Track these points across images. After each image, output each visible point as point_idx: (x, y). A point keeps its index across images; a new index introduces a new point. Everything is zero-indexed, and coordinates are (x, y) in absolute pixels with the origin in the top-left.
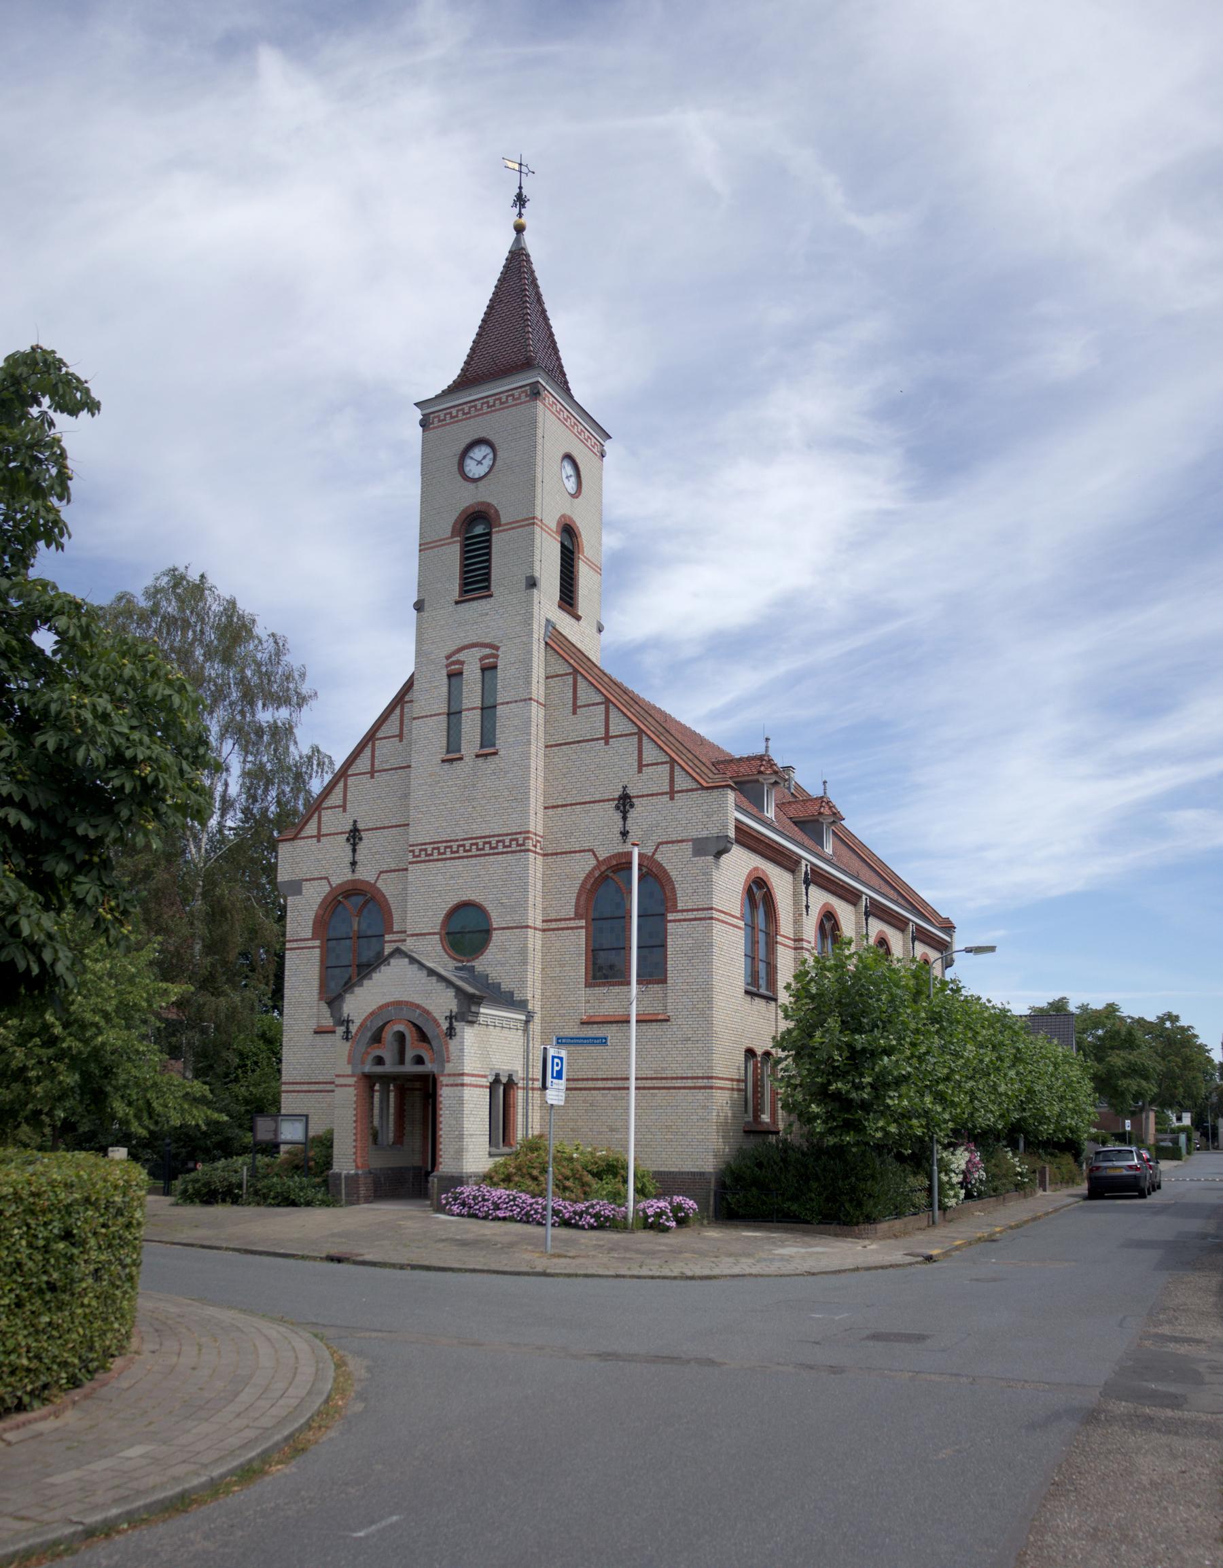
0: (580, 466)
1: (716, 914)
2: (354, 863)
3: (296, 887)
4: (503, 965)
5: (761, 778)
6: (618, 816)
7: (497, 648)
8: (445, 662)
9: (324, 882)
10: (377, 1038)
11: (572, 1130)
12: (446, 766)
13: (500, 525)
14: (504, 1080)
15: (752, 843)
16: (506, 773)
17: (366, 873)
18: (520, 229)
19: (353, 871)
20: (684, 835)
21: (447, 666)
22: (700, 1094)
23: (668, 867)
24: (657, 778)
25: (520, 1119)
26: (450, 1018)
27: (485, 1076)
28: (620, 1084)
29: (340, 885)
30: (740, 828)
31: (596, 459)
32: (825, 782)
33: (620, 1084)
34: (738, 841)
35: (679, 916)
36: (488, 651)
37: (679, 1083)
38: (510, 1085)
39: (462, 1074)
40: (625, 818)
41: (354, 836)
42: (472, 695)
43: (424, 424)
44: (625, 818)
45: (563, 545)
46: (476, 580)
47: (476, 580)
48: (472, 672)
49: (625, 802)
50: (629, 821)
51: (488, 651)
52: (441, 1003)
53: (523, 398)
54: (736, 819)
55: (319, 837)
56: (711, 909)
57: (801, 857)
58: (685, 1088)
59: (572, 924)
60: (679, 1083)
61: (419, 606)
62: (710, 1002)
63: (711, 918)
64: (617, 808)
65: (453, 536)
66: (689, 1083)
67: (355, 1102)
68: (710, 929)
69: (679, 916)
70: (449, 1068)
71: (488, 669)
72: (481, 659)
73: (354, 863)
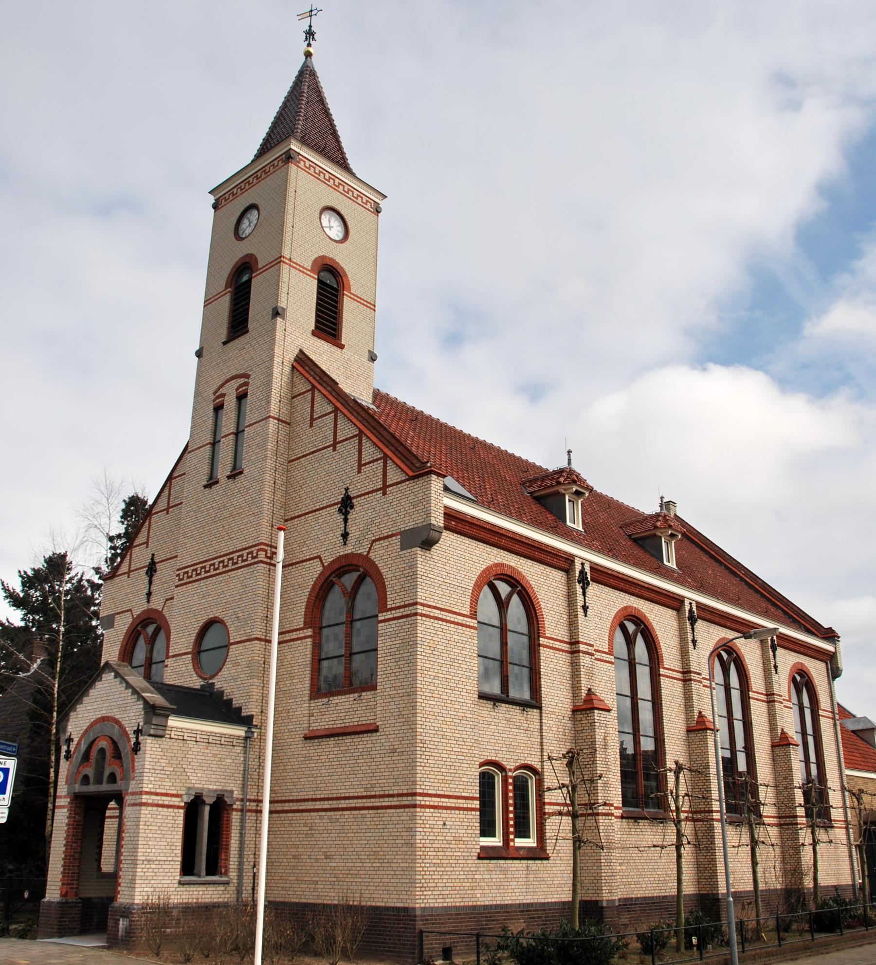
0: (342, 213)
1: (420, 609)
2: (149, 594)
3: (109, 622)
4: (235, 680)
5: (561, 489)
6: (340, 518)
7: (247, 376)
8: (213, 397)
9: (128, 614)
10: (86, 756)
11: (294, 857)
12: (207, 491)
13: (258, 270)
14: (210, 800)
15: (488, 537)
16: (249, 489)
17: (157, 603)
18: (308, 55)
19: (148, 602)
20: (394, 530)
21: (214, 401)
22: (405, 814)
23: (380, 565)
24: (372, 475)
25: (234, 843)
26: (138, 732)
27: (177, 796)
28: (279, 807)
29: (139, 615)
30: (450, 515)
31: (373, 216)
32: (569, 452)
33: (279, 807)
34: (446, 528)
35: (389, 615)
36: (242, 381)
37: (386, 802)
38: (220, 807)
39: (141, 793)
40: (346, 520)
41: (151, 569)
42: (228, 423)
43: (215, 207)
44: (346, 520)
45: (320, 282)
46: (238, 324)
47: (238, 324)
48: (230, 402)
49: (346, 505)
50: (350, 523)
51: (242, 381)
52: (132, 716)
53: (280, 164)
54: (446, 507)
55: (129, 573)
56: (416, 604)
57: (572, 556)
58: (391, 807)
59: (301, 634)
60: (386, 802)
61: (199, 354)
62: (414, 708)
63: (416, 614)
64: (340, 510)
65: (226, 289)
66: (395, 801)
67: (68, 825)
68: (414, 626)
69: (389, 615)
70: (133, 787)
71: (241, 397)
72: (237, 390)
73: (149, 594)
